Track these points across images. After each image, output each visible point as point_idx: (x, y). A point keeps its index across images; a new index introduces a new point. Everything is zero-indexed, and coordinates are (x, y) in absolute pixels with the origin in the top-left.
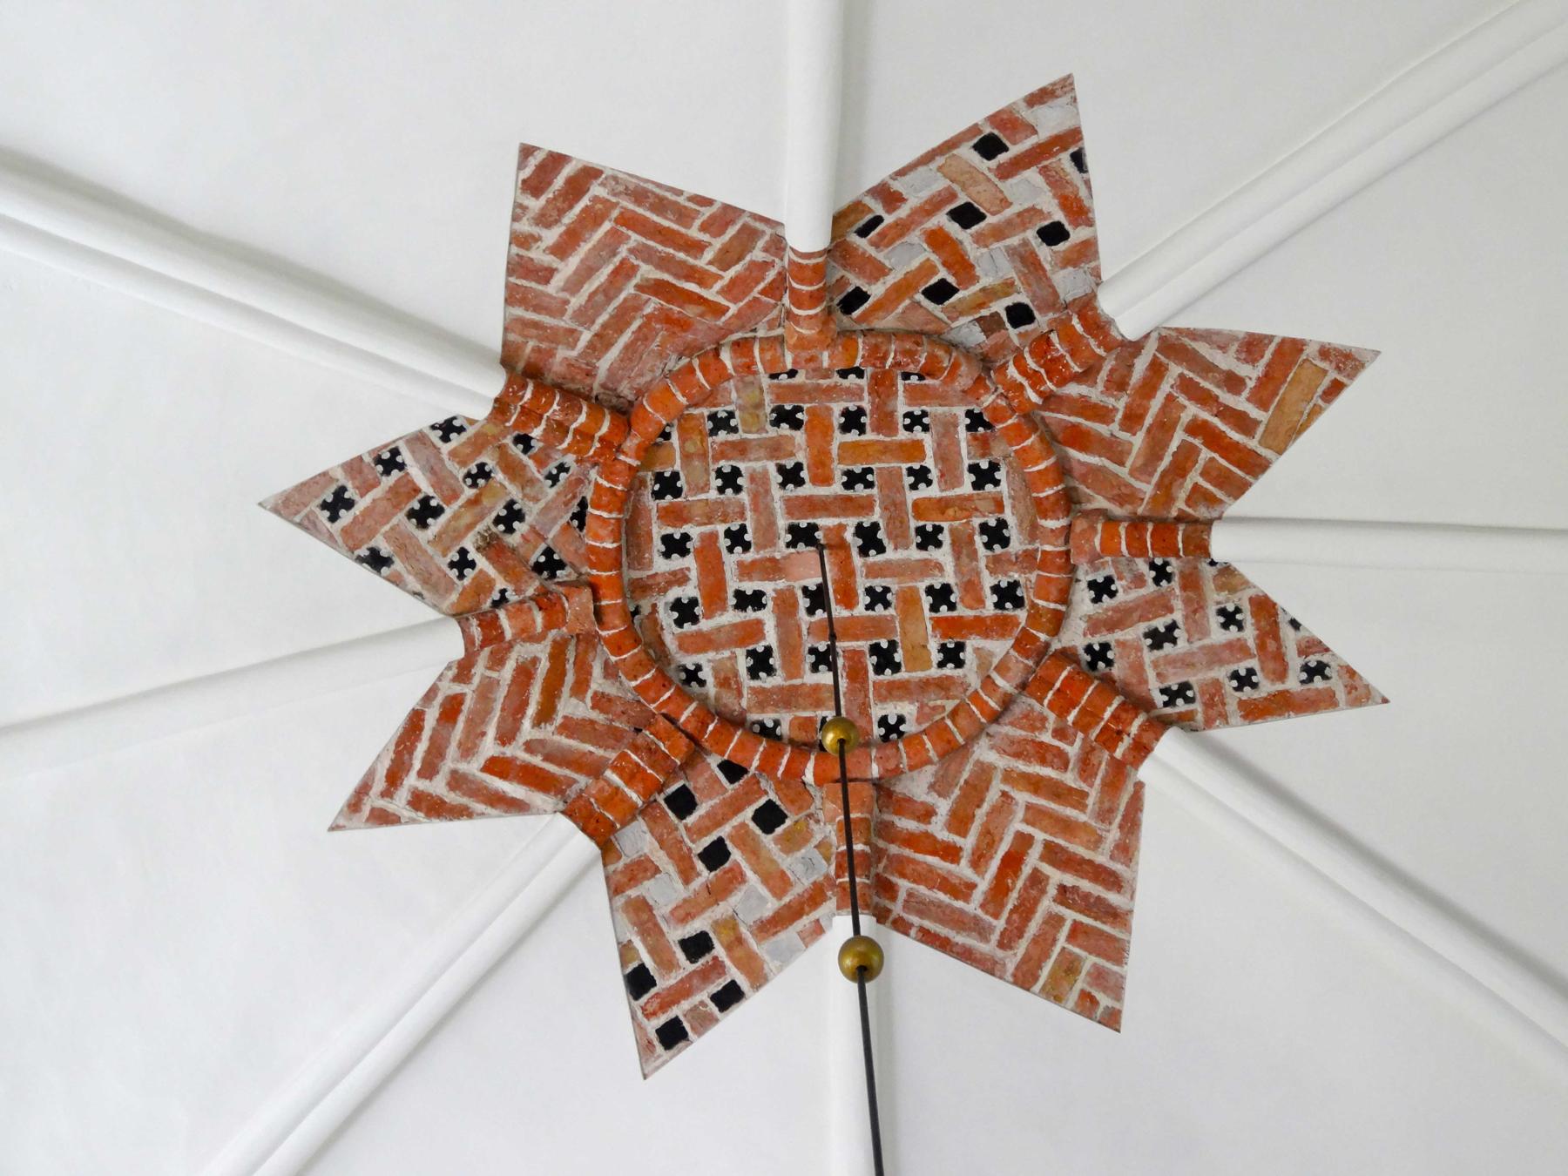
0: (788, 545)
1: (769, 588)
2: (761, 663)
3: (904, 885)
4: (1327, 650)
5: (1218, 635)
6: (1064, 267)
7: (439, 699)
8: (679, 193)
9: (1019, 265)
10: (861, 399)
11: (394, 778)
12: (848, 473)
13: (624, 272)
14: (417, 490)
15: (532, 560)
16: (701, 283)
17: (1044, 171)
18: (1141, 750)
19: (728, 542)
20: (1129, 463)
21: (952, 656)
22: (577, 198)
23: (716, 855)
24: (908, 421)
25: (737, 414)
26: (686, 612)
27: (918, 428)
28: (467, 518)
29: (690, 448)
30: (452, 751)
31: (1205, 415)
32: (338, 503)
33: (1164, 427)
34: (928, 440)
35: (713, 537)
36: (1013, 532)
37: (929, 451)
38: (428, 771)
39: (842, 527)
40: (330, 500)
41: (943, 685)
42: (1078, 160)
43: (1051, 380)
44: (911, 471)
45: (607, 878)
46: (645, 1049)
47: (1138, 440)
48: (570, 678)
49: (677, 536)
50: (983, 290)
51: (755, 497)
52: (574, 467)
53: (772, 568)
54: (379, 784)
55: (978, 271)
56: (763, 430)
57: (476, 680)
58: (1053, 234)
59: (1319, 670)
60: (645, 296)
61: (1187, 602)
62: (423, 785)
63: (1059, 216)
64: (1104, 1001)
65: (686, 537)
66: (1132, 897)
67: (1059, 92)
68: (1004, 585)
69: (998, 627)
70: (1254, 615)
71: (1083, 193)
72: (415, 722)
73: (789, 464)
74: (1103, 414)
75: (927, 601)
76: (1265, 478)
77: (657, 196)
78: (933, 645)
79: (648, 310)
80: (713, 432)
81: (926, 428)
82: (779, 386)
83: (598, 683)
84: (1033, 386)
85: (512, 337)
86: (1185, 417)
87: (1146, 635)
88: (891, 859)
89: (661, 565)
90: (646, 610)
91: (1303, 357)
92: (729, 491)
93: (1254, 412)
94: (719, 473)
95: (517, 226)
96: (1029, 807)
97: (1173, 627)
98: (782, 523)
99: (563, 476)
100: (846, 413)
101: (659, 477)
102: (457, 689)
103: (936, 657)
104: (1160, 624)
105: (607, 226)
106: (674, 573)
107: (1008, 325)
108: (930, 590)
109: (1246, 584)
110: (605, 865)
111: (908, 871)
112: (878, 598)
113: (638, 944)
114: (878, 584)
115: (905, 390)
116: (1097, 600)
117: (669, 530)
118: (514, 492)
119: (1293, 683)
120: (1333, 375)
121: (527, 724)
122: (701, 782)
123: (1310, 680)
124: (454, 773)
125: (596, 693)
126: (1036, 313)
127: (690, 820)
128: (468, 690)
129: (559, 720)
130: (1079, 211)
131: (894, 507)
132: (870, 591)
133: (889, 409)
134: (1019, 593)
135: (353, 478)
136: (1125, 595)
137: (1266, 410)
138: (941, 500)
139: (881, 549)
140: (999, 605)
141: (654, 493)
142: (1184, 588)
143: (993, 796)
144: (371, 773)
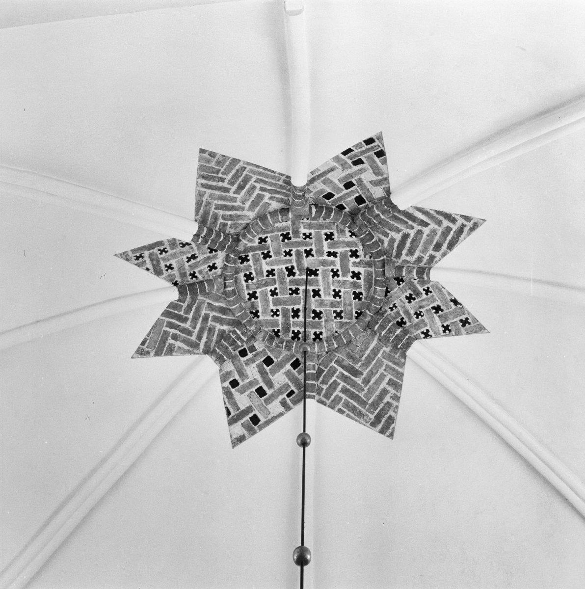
0: (318, 270)
1: (325, 257)
2: (329, 237)
4: (136, 265)
5: (174, 263)
6: (231, 371)
7: (441, 252)
8: (348, 416)
9: (245, 372)
10: (293, 322)
11: (460, 231)
12: (298, 294)
13: (366, 381)
14: (439, 316)
15: (404, 283)
16: (343, 374)
17: (238, 409)
19: (338, 273)
20: (206, 304)
21: (263, 240)
22: (378, 414)
24: (278, 313)
25: (333, 318)
26: (354, 254)
27: (275, 311)
28: (424, 303)
29: (349, 308)
30: (439, 233)
31: (182, 325)
32: (465, 322)
33: (195, 319)
34: (272, 307)
35: (344, 275)
36: (243, 279)
37: (271, 303)
38: (448, 229)
39: (300, 275)
40: (467, 324)
42: (229, 413)
43: (233, 339)
44: (277, 294)
45: (389, 183)
46: (380, 137)
47: (204, 312)
48: (396, 245)
49: (355, 278)
50: (255, 362)
51: (329, 287)
52: (387, 308)
53: (324, 263)
54: (466, 229)
55: (257, 369)
56: (326, 311)
57: (428, 254)
58: (234, 384)
60: (360, 369)
61: (184, 269)
62: (451, 225)
63: (233, 390)
64: (206, 155)
65: (352, 277)
66: (197, 182)
67: (236, 440)
68: (245, 262)
70: (162, 270)
71: (226, 400)
72: (451, 246)
73: (317, 297)
74: (216, 319)
77: (354, 414)
79: (360, 364)
80: (341, 312)
81: (272, 311)
82: (319, 328)
83: (386, 241)
84: (239, 335)
85: (403, 360)
86: (189, 323)
87: (197, 257)
88: (285, 189)
89: (362, 270)
90: (368, 256)
91: (154, 351)
92: (337, 290)
93: (168, 329)
94: (340, 297)
95: (397, 404)
98: (320, 277)
99: (391, 306)
100: (298, 316)
101: (360, 299)
102: (435, 253)
104: (193, 261)
105: (370, 402)
106: (357, 266)
107: (247, 349)
108: (270, 257)
109: (165, 279)
110: (389, 187)
111: (279, 186)
112: (288, 253)
113: (379, 164)
114: (288, 257)
115: (279, 325)
116: (214, 264)
117: (358, 281)
118: (408, 306)
119: (146, 254)
120: (144, 347)
121: (412, 235)
122: (352, 204)
123: (141, 255)
124: (440, 226)
125: (387, 237)
126: (238, 354)
127: (357, 195)
128: (431, 251)
129: (401, 233)
130: (228, 394)
131: (282, 283)
132: (291, 255)
133: (284, 318)
134: (240, 261)
135: (459, 328)
136: (205, 267)
137: (164, 331)
138: (267, 286)
139: (287, 268)
141: (362, 295)
142: (185, 273)
144: (468, 234)
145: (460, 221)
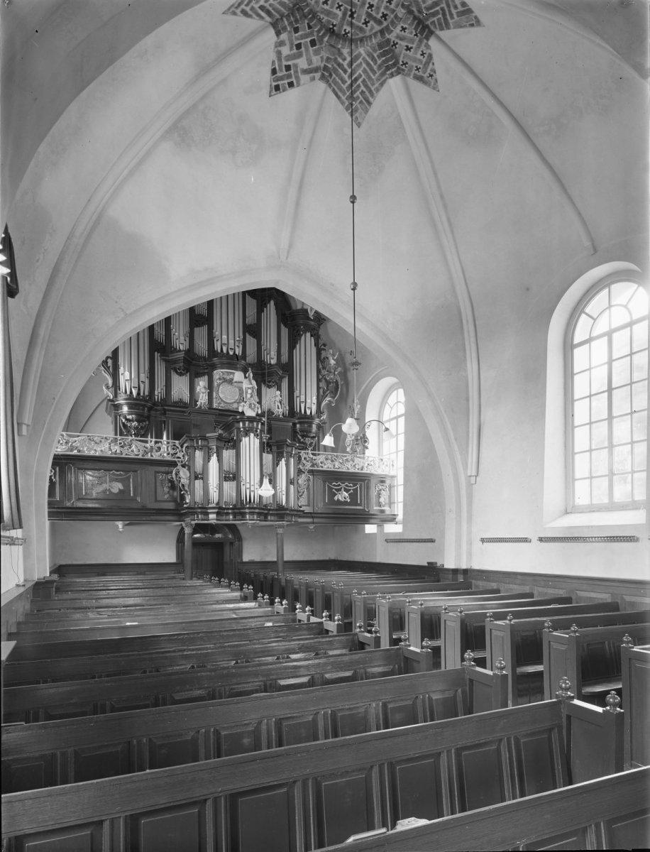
3: (334, 76)
18: (392, 75)
21: (366, 23)
23: (299, 46)
41: (361, 29)
59: (431, 76)
61: (418, 44)
62: (245, 8)
69: (380, 23)
75: (367, 5)
76: (448, 31)
78: (364, 17)
86: (442, 6)
93: (455, 16)
96: (364, 68)
97: (411, 48)
103: (363, 21)
113: (276, 61)
127: (297, 35)
140: (382, 17)
142: (419, 41)
143: (358, 62)
145: (238, 11)
